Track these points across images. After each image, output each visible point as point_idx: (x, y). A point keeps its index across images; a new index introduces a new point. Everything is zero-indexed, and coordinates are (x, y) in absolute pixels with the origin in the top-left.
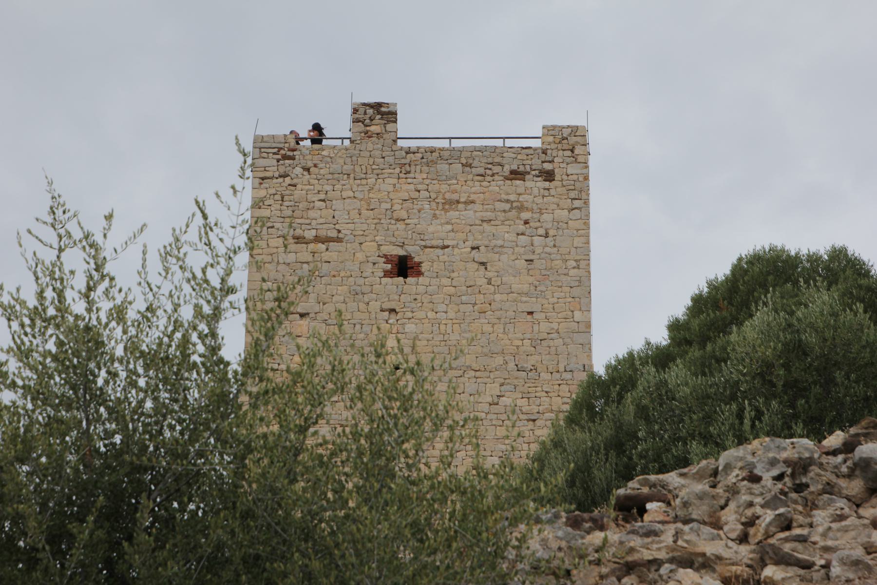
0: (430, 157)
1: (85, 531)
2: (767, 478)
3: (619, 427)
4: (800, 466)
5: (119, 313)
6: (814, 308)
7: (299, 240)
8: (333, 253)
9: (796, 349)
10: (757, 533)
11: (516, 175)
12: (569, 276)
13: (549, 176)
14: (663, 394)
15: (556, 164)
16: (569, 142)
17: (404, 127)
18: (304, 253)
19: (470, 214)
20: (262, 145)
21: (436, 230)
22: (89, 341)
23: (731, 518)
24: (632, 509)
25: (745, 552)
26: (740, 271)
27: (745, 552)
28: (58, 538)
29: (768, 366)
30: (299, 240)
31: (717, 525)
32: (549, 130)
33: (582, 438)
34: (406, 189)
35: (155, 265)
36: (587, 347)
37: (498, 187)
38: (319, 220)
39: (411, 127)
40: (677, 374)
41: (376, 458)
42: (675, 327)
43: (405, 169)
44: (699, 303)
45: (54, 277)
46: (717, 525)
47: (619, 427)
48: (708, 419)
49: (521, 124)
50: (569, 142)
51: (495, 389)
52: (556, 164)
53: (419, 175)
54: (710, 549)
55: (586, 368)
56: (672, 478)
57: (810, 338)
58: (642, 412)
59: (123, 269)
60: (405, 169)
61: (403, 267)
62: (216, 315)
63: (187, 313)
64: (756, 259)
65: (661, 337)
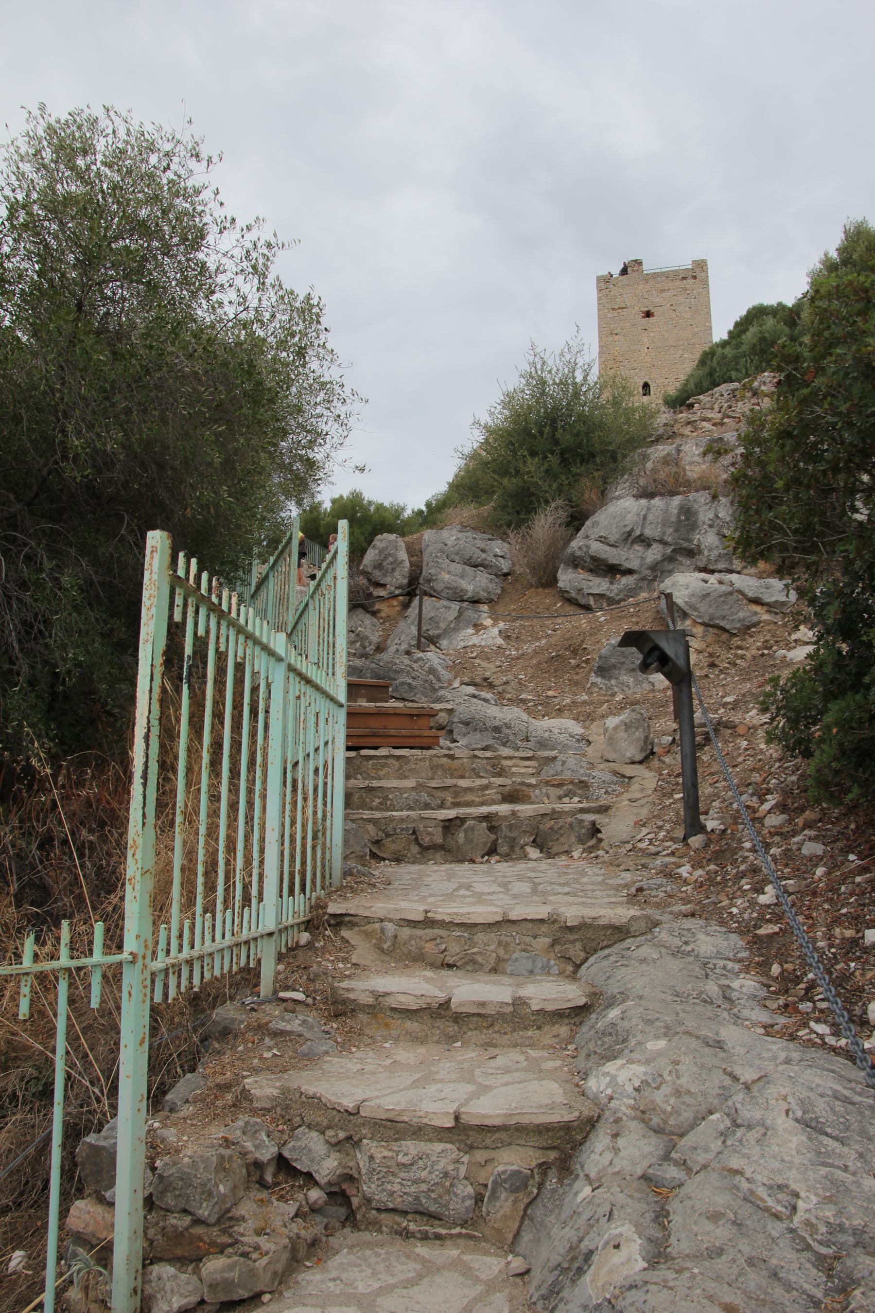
0: (655, 276)
1: (547, 430)
2: (725, 395)
3: (711, 367)
4: (734, 391)
5: (550, 372)
6: (769, 324)
7: (613, 309)
8: (624, 312)
9: (763, 339)
10: (723, 410)
11: (684, 278)
12: (703, 311)
13: (695, 278)
14: (724, 357)
15: (697, 273)
16: (701, 265)
17: (645, 267)
18: (615, 313)
19: (669, 294)
20: (599, 279)
21: (658, 300)
22: (543, 382)
23: (716, 407)
24: (691, 406)
25: (720, 415)
26: (749, 312)
27: (720, 415)
28: (541, 433)
29: (755, 345)
30: (613, 309)
31: (712, 409)
32: (694, 262)
33: (700, 373)
34: (648, 288)
35: (557, 359)
36: (711, 335)
37: (678, 283)
38: (619, 302)
39: (648, 267)
40: (728, 351)
41: (616, 403)
42: (730, 332)
43: (647, 281)
44: (737, 325)
45: (534, 364)
46: (712, 409)
47: (711, 367)
48: (737, 363)
49: (683, 261)
50: (701, 265)
51: (681, 352)
52: (697, 273)
53: (651, 283)
54: (710, 416)
55: (711, 342)
56: (701, 397)
57: (767, 335)
58: (718, 363)
59: (550, 362)
60: (647, 281)
61: (648, 314)
62: (574, 371)
63: (566, 370)
64: (754, 308)
65: (725, 337)
